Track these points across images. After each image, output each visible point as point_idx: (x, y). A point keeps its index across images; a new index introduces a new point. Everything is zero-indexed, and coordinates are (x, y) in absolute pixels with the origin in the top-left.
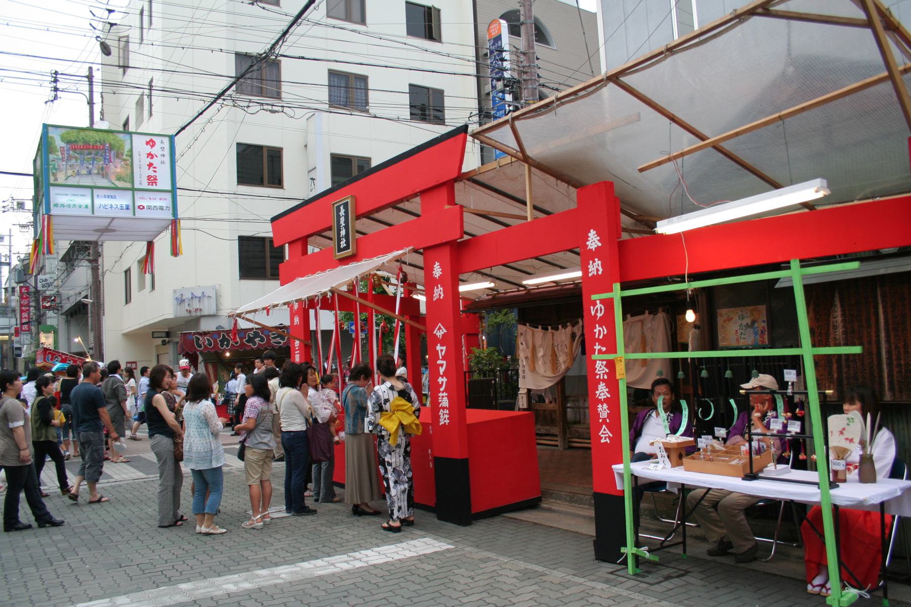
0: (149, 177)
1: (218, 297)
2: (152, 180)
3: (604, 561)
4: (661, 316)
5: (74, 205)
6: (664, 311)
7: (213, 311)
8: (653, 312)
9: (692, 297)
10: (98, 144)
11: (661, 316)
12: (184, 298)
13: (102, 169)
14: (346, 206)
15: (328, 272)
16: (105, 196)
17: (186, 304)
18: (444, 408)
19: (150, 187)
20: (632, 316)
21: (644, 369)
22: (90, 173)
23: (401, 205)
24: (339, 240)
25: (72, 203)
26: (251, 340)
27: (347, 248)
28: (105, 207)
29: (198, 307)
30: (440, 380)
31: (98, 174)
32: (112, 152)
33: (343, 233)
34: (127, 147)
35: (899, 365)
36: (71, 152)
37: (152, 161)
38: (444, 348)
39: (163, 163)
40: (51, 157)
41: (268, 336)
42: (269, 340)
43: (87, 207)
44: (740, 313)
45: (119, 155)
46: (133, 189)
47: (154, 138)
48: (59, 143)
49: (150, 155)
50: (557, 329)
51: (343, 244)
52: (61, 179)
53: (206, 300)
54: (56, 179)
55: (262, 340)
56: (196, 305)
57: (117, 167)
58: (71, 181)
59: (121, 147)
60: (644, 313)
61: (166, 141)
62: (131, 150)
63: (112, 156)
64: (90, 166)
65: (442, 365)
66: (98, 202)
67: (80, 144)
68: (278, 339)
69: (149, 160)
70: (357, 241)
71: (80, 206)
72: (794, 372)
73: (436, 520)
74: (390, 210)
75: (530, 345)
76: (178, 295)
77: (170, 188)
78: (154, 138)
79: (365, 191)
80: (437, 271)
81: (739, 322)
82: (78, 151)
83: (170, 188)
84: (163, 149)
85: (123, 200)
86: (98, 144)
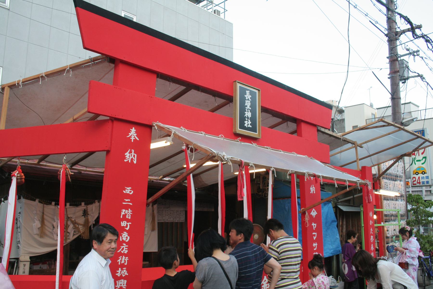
30: (314, 245)
38: (316, 225)
65: (315, 235)
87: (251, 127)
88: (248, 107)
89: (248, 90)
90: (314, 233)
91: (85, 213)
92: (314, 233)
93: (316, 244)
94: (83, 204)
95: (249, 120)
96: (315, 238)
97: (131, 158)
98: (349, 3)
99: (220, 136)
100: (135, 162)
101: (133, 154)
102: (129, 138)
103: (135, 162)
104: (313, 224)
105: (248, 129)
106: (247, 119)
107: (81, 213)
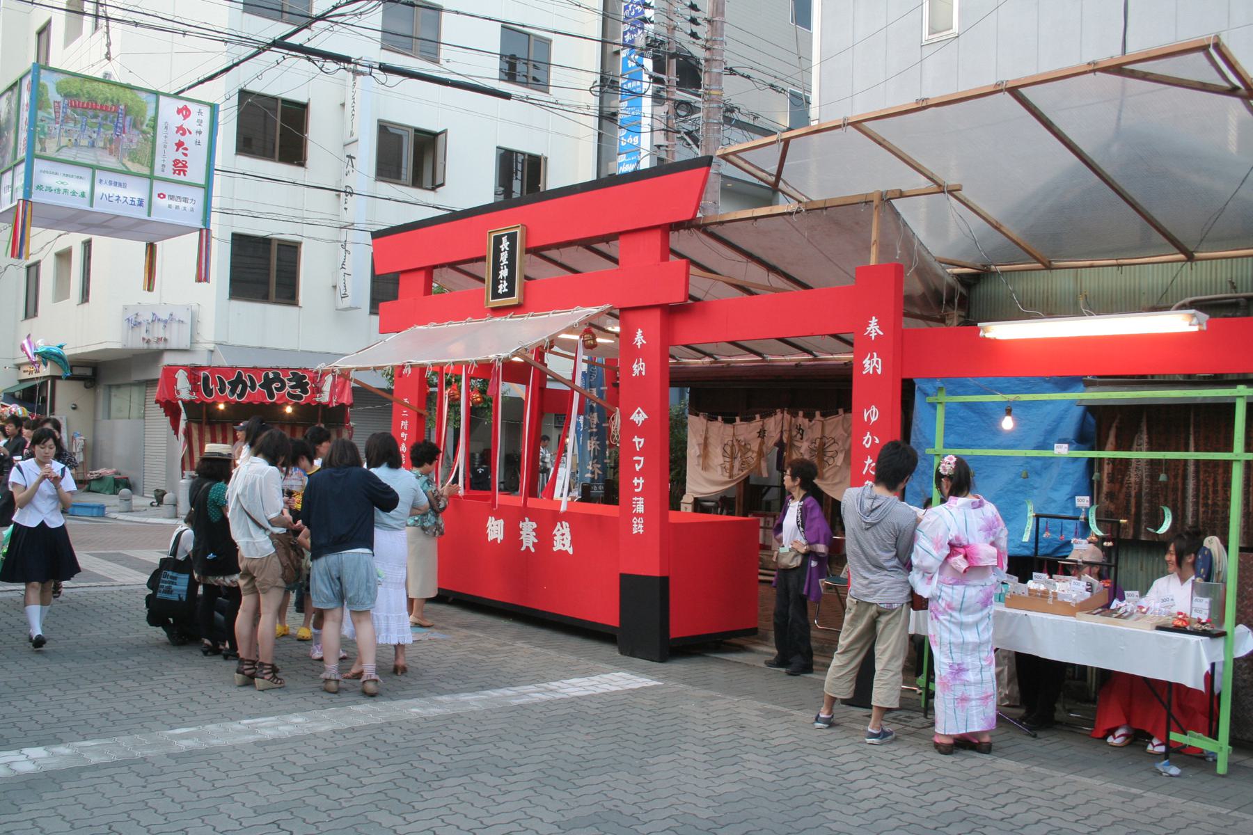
0: (176, 162)
1: (195, 322)
2: (180, 167)
3: (633, 654)
5: (66, 191)
7: (185, 344)
9: (1136, 430)
10: (110, 104)
12: (139, 320)
13: (111, 141)
14: (512, 238)
15: (468, 325)
16: (110, 183)
17: (143, 329)
18: (638, 515)
19: (176, 177)
22: (93, 145)
23: (602, 247)
24: (496, 282)
25: (62, 187)
27: (510, 293)
28: (109, 198)
29: (161, 335)
30: (636, 481)
31: (104, 148)
32: (128, 118)
33: (504, 273)
34: (150, 113)
35: (1206, 505)
36: (69, 111)
37: (183, 139)
38: (642, 440)
39: (198, 143)
40: (41, 114)
43: (83, 195)
45: (135, 125)
46: (151, 177)
47: (190, 106)
48: (53, 95)
49: (182, 130)
51: (503, 288)
52: (51, 150)
53: (175, 326)
54: (43, 149)
56: (159, 331)
57: (132, 139)
58: (66, 155)
59: (141, 112)
61: (206, 111)
62: (155, 119)
63: (127, 123)
64: (95, 136)
65: (639, 462)
66: (100, 190)
67: (84, 100)
69: (178, 137)
71: (74, 193)
72: (1087, 498)
73: (618, 654)
76: (131, 315)
77: (203, 182)
78: (190, 106)
79: (543, 222)
80: (639, 339)
82: (79, 110)
83: (203, 182)
84: (200, 122)
85: (134, 190)
86: (110, 104)
88: (505, 262)
90: (636, 458)
91: (762, 434)
92: (636, 458)
93: (641, 481)
94: (758, 416)
96: (638, 468)
98: (941, 189)
100: (879, 372)
101: (875, 359)
102: (869, 337)
103: (879, 372)
104: (636, 439)
105: (505, 295)
107: (755, 434)
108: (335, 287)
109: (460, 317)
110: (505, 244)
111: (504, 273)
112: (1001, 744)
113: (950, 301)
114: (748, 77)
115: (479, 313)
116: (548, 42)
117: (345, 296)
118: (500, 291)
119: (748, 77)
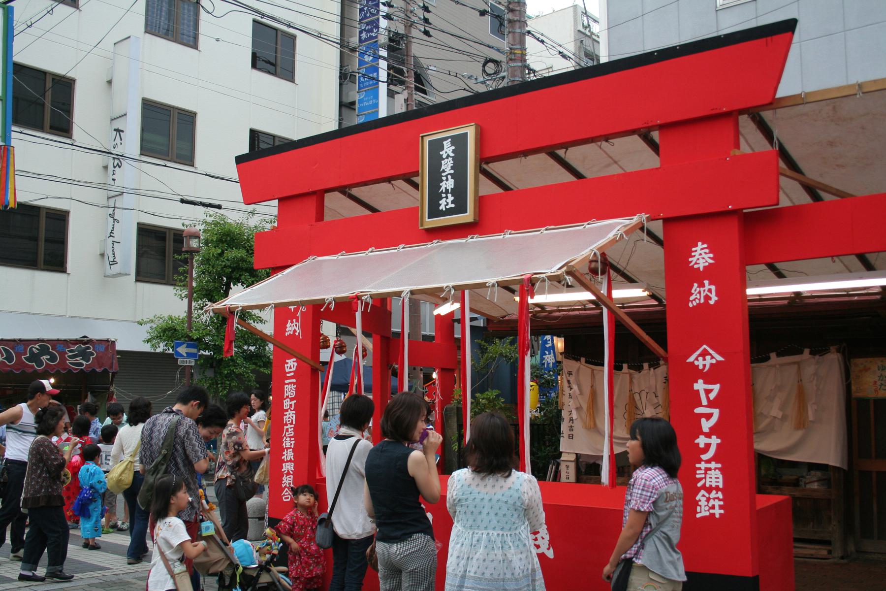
4: (833, 358)
6: (838, 351)
8: (819, 350)
11: (833, 358)
14: (460, 142)
20: (778, 355)
21: (799, 434)
26: (34, 357)
27: (460, 207)
41: (62, 354)
42: (63, 359)
44: (880, 364)
50: (639, 369)
55: (53, 358)
60: (801, 352)
65: (708, 416)
68: (79, 360)
70: (481, 201)
74: (543, 156)
75: (587, 391)
81: (879, 373)
87: (453, 206)
88: (449, 170)
89: (446, 139)
95: (450, 195)
97: (703, 295)
99: (370, 250)
101: (707, 287)
105: (449, 212)
106: (444, 195)
108: (102, 255)
109: (392, 243)
110: (448, 149)
111: (448, 184)
112: (341, 518)
113: (594, 272)
114: (542, 42)
115: (410, 240)
116: (293, 38)
117: (114, 262)
118: (442, 207)
119: (542, 42)
